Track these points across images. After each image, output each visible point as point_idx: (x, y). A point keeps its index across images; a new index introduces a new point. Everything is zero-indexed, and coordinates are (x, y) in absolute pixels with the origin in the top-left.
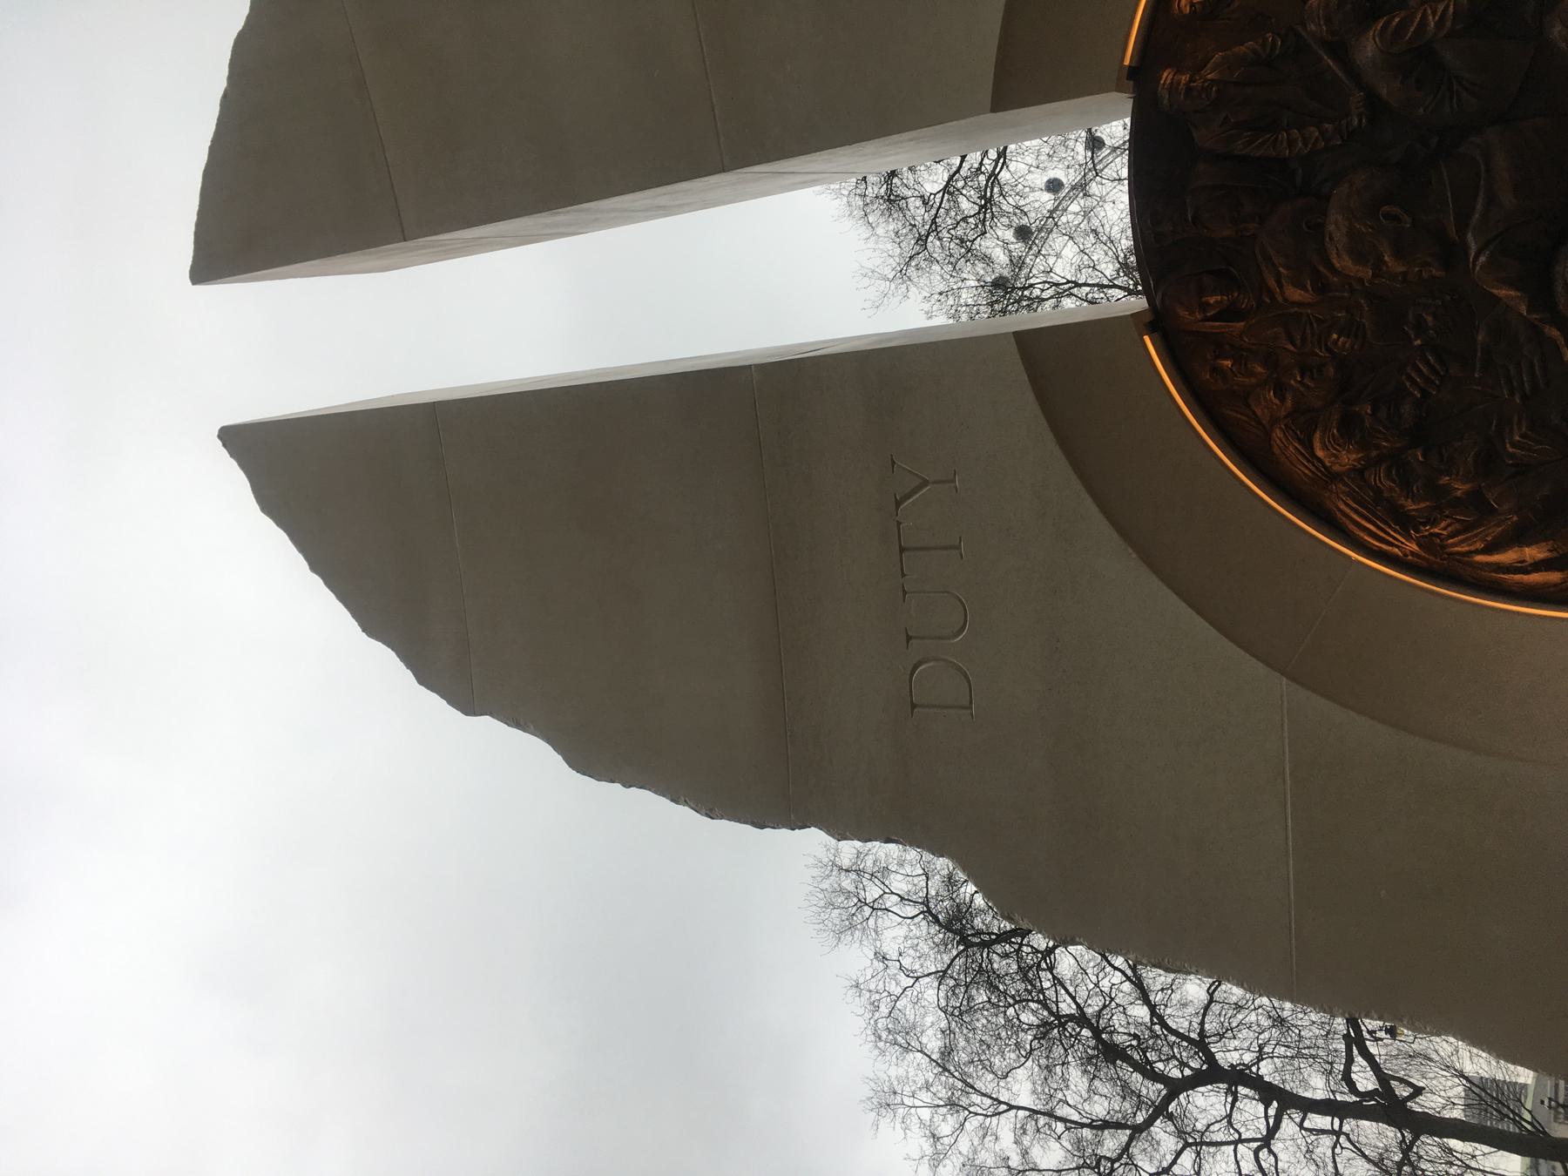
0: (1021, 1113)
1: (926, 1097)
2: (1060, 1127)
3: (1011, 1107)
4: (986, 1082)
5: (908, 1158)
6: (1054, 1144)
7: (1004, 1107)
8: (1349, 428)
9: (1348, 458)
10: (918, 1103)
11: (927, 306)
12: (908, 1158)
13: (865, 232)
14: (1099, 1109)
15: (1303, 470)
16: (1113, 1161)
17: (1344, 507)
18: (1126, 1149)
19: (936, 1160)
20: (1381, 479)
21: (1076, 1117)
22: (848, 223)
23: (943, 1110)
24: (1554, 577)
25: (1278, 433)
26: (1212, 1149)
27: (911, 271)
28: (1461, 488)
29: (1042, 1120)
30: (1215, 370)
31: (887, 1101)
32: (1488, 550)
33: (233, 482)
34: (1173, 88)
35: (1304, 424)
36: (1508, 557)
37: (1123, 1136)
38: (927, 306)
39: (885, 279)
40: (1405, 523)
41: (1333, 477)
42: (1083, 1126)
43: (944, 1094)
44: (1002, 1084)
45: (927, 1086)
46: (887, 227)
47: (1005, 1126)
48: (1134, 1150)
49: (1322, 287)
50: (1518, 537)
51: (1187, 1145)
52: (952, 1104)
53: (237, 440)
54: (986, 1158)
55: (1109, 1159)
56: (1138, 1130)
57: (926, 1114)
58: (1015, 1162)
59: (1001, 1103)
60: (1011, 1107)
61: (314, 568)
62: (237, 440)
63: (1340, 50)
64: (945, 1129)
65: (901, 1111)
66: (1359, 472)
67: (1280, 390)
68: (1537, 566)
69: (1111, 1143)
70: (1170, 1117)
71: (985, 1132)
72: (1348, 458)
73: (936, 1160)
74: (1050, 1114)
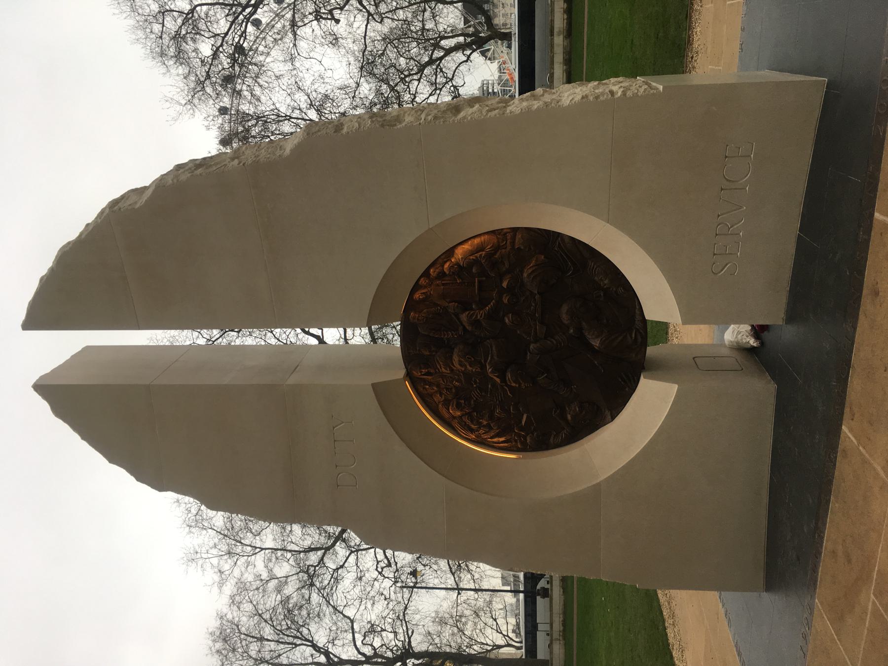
0: (267, 551)
1: (215, 551)
2: (289, 555)
3: (262, 549)
4: (248, 539)
5: (206, 585)
6: (285, 564)
7: (258, 550)
8: (459, 407)
9: (459, 413)
10: (210, 556)
11: (206, 123)
12: (206, 585)
13: (163, 69)
14: (307, 543)
15: (447, 416)
16: (315, 567)
17: (457, 426)
18: (322, 559)
19: (221, 584)
20: (465, 419)
21: (297, 549)
22: (150, 63)
23: (226, 557)
24: (506, 445)
25: (440, 406)
26: (364, 552)
27: (196, 101)
28: (485, 423)
29: (279, 553)
30: (424, 388)
31: (193, 557)
32: (491, 438)
33: (44, 406)
34: (414, 318)
35: (447, 403)
36: (495, 440)
37: (320, 553)
38: (206, 123)
39: (181, 104)
40: (472, 431)
41: (454, 418)
42: (300, 552)
43: (225, 548)
44: (257, 538)
45: (215, 546)
46: (182, 70)
47: (259, 560)
48: (325, 560)
49: (452, 370)
50: (498, 435)
51: (352, 552)
52: (229, 553)
53: (43, 388)
54: (249, 577)
55: (312, 566)
56: (327, 549)
57: (215, 561)
58: (265, 576)
59: (256, 548)
60: (262, 549)
61: (83, 438)
62: (43, 388)
63: (457, 315)
64: (226, 567)
65: (200, 562)
66: (461, 417)
67: (441, 395)
68: (502, 442)
69: (314, 558)
70: (344, 540)
71: (248, 564)
72: (459, 413)
73: (221, 584)
74: (284, 549)
